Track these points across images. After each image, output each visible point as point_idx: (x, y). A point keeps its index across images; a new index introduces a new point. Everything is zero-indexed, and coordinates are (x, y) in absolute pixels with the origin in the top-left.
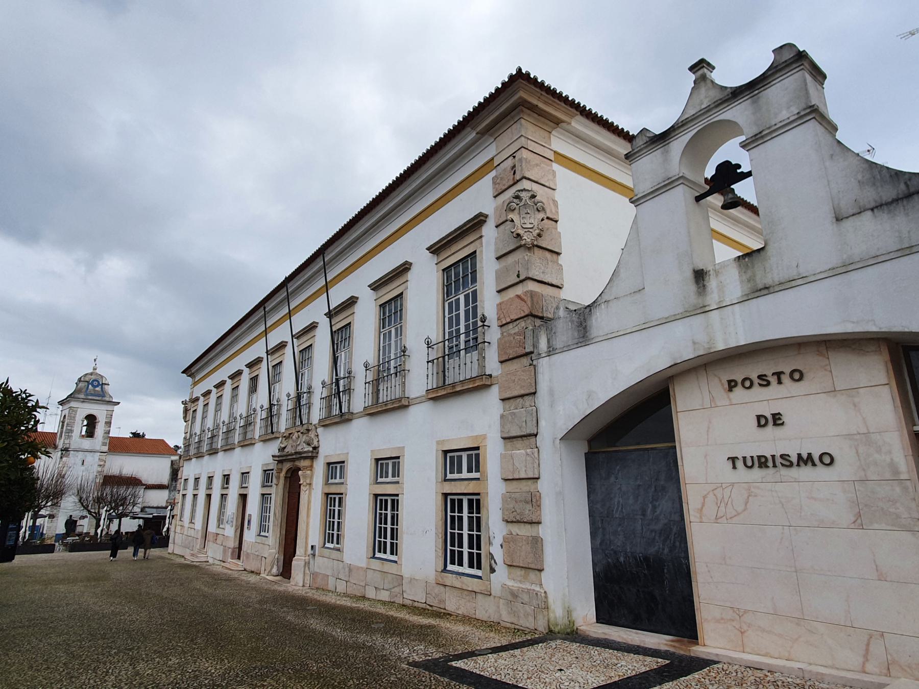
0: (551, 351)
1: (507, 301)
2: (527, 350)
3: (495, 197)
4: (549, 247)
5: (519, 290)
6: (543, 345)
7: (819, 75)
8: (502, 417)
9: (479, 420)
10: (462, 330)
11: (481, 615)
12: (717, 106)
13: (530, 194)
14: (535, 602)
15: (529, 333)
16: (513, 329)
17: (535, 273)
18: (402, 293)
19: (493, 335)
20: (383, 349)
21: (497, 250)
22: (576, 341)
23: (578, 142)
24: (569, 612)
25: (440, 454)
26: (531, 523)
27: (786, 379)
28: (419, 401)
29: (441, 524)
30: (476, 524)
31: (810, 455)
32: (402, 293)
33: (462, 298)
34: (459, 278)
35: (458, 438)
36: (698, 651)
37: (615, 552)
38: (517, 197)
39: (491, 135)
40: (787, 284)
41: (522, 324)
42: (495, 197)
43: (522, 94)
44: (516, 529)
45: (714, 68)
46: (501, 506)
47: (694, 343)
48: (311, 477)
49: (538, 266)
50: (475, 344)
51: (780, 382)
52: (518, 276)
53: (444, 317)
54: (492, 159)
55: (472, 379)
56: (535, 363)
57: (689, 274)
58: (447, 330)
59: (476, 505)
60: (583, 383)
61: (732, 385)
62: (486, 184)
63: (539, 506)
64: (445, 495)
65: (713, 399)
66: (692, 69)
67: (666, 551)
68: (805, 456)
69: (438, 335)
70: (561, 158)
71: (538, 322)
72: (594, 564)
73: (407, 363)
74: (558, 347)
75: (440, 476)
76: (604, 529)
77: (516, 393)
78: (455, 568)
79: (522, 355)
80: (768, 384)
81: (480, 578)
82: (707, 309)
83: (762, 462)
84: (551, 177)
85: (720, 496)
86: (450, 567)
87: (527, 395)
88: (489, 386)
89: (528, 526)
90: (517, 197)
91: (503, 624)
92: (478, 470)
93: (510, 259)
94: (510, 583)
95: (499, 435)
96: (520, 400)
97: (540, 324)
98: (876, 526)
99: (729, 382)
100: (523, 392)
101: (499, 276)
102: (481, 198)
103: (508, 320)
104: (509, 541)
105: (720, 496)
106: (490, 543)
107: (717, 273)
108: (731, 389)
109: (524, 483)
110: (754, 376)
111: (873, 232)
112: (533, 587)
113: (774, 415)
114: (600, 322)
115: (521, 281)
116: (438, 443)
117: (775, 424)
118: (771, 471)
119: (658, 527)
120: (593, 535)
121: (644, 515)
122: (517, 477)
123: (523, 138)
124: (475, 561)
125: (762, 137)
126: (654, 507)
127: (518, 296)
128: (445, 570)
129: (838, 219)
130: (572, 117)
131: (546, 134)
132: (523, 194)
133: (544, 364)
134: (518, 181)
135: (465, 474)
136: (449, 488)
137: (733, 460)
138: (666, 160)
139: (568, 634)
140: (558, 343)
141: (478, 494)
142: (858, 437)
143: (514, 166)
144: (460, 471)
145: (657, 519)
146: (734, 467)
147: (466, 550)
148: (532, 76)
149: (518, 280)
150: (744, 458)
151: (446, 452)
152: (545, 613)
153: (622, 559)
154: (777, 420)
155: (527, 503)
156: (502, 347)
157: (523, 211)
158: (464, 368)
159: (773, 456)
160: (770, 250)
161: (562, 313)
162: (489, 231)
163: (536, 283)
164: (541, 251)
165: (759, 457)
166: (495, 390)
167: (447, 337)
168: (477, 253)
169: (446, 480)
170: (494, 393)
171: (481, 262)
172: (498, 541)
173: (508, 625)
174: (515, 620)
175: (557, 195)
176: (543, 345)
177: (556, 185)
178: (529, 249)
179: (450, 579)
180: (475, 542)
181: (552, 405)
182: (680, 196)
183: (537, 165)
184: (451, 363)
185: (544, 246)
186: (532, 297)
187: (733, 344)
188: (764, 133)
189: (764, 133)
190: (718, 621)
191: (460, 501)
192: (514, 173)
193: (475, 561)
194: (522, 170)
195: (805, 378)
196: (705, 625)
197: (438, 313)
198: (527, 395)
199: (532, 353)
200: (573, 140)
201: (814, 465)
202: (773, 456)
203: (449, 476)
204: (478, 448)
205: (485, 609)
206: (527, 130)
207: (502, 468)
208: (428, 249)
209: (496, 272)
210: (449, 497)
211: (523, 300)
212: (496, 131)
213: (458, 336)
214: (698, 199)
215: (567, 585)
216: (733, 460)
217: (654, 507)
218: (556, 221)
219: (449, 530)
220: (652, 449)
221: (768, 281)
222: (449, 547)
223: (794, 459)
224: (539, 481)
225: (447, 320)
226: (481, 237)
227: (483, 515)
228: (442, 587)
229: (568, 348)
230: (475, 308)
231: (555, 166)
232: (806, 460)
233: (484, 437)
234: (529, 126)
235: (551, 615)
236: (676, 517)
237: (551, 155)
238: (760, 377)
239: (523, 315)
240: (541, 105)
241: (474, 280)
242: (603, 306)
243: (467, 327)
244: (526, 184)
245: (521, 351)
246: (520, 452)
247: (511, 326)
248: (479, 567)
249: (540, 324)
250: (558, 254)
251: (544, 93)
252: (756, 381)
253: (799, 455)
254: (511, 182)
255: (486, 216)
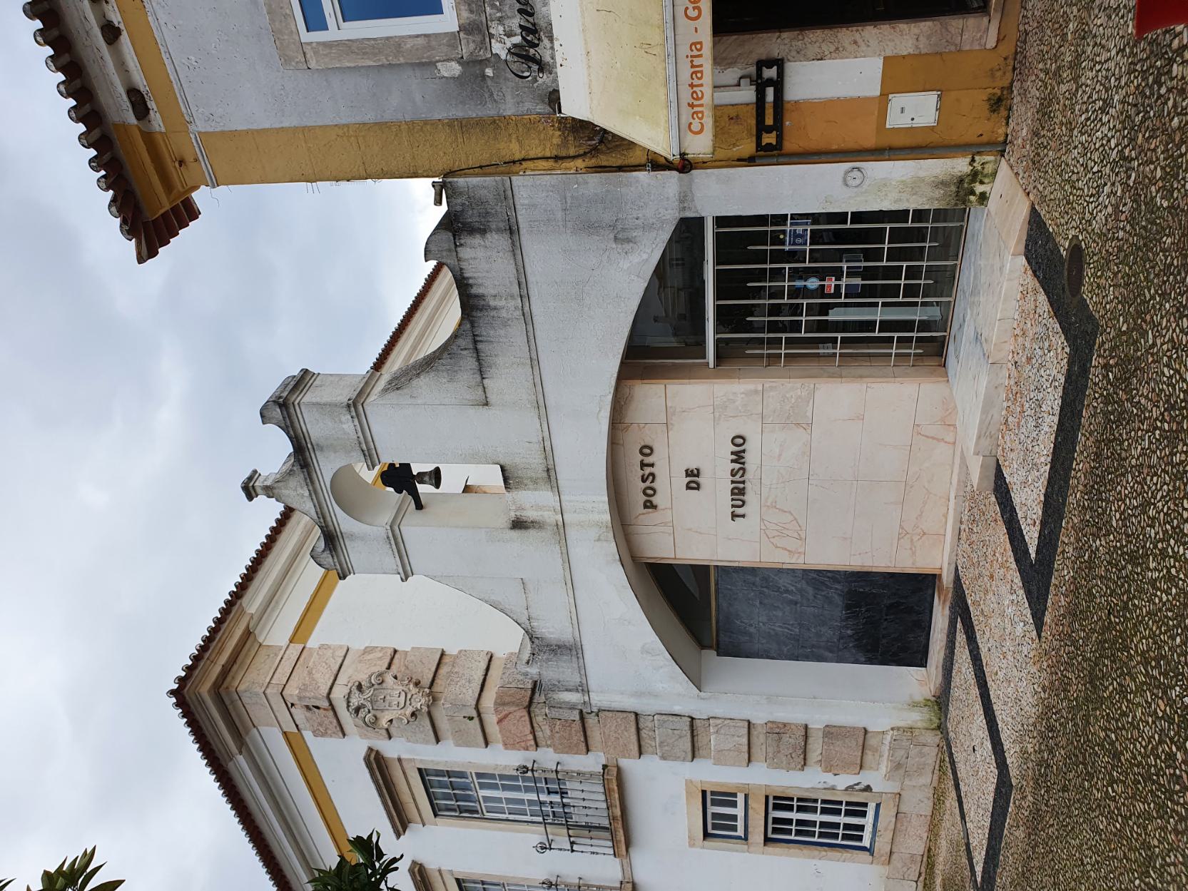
0: (583, 688)
1: (503, 736)
2: (577, 718)
3: (344, 735)
4: (433, 669)
5: (491, 719)
6: (574, 697)
7: (302, 380)
8: (663, 758)
9: (665, 791)
10: (533, 797)
11: (926, 808)
12: (312, 483)
13: (356, 692)
14: (906, 743)
15: (554, 713)
16: (544, 731)
17: (470, 695)
18: (458, 880)
19: (547, 758)
21: (427, 742)
22: (574, 659)
23: (277, 603)
24: (914, 705)
25: (709, 843)
26: (806, 737)
27: (648, 460)
28: (627, 867)
29: (807, 851)
30: (806, 805)
31: (732, 453)
32: (458, 880)
33: (483, 793)
34: (452, 796)
35: (688, 818)
36: (947, 579)
37: (841, 638)
38: (357, 710)
39: (247, 732)
40: (547, 452)
41: (539, 719)
42: (344, 735)
43: (205, 689)
44: (814, 755)
45: (255, 472)
46: (784, 771)
47: (599, 540)
49: (458, 690)
50: (556, 783)
51: (652, 465)
52: (471, 718)
53: (508, 820)
54: (285, 733)
55: (607, 792)
56: (595, 710)
57: (516, 534)
58: (528, 818)
59: (782, 802)
60: (627, 654)
61: (649, 505)
62: (322, 749)
63: (785, 725)
65: (665, 524)
66: (250, 498)
68: (734, 457)
69: (534, 832)
70: (301, 632)
71: (539, 698)
72: (856, 662)
73: (569, 881)
74: (578, 680)
75: (740, 846)
76: (813, 646)
77: (634, 738)
78: (867, 835)
79: (583, 726)
80: (653, 475)
81: (878, 806)
82: (560, 523)
83: (738, 492)
84: (329, 653)
85: (776, 533)
86: (866, 842)
87: (637, 724)
88: (619, 770)
89: (810, 740)
90: (357, 710)
91: (935, 784)
92: (735, 795)
93: (443, 724)
94: (883, 769)
95: (688, 764)
96: (644, 733)
97: (539, 695)
98: (809, 414)
99: (646, 507)
100: (633, 729)
101: (463, 741)
102: (341, 759)
103: (531, 737)
104: (829, 765)
105: (776, 533)
106: (833, 788)
107: (521, 508)
108: (654, 507)
109: (754, 739)
110: (643, 485)
111: (507, 379)
112: (887, 742)
113: (687, 475)
114: (554, 627)
115: (479, 715)
116: (692, 845)
117: (698, 476)
118: (748, 485)
119: (810, 590)
120: (820, 659)
121: (796, 603)
122: (746, 748)
123: (268, 691)
124: (857, 810)
125: (369, 450)
126: (787, 591)
127: (500, 721)
128: (869, 850)
129: (487, 404)
130: (243, 611)
131: (263, 652)
132: (355, 702)
133: (598, 700)
134: (331, 704)
135: (739, 811)
136: (757, 835)
137: (734, 516)
138: (362, 538)
139: (940, 709)
140: (573, 678)
141: (767, 797)
142: (717, 414)
143: (307, 707)
144: (734, 818)
145: (801, 591)
146: (743, 516)
147: (842, 819)
148: (183, 674)
149: (476, 720)
150: (733, 506)
151: (706, 835)
152: (916, 733)
153: (849, 632)
154: (693, 474)
155: (780, 739)
156: (569, 749)
157: (380, 705)
158: (589, 801)
159: (733, 482)
160: (506, 461)
162: (391, 749)
163: (485, 694)
164: (437, 681)
165: (733, 494)
166: (625, 763)
167: (540, 819)
169: (746, 839)
170: (631, 766)
171: (438, 763)
172: (830, 779)
173: (936, 777)
174: (929, 769)
175: (357, 645)
176: (574, 697)
177: (341, 647)
178: (434, 699)
179: (882, 845)
180: (831, 807)
181: (656, 696)
182: (415, 530)
183: (310, 673)
184: (578, 817)
185: (431, 676)
186: (504, 704)
187: (607, 507)
188: (364, 448)
189: (364, 448)
190: (914, 553)
191: (776, 820)
192: (317, 708)
193: (857, 810)
194: (316, 698)
195: (650, 444)
196: (919, 565)
197: (500, 829)
198: (637, 724)
199: (581, 712)
200: (273, 610)
201: (744, 451)
202: (733, 482)
203: (740, 832)
204: (704, 792)
205: (918, 803)
206: (253, 683)
207: (733, 765)
208: (398, 836)
209: (458, 745)
210: (770, 835)
211: (506, 716)
212: (242, 721)
213: (542, 803)
214: (419, 506)
215: (881, 698)
216: (734, 516)
217: (787, 591)
218: (395, 651)
219: (816, 839)
220: (717, 584)
221: (542, 468)
222: (839, 841)
223: (737, 466)
224: (753, 721)
225: (511, 817)
226: (399, 760)
227: (796, 794)
228: (894, 857)
229: (582, 670)
230: (502, 777)
231: (313, 643)
232: (739, 457)
233: (689, 783)
234: (252, 676)
235: (920, 725)
237: (295, 649)
238: (644, 480)
239: (527, 718)
240: (223, 659)
241: (462, 775)
242: (535, 624)
243: (527, 790)
244: (339, 694)
245: (578, 725)
246: (713, 740)
247: (539, 734)
248: (866, 805)
249: (539, 695)
250: (443, 654)
251: (207, 655)
252: (648, 484)
253: (733, 461)
254: (331, 713)
255: (370, 749)
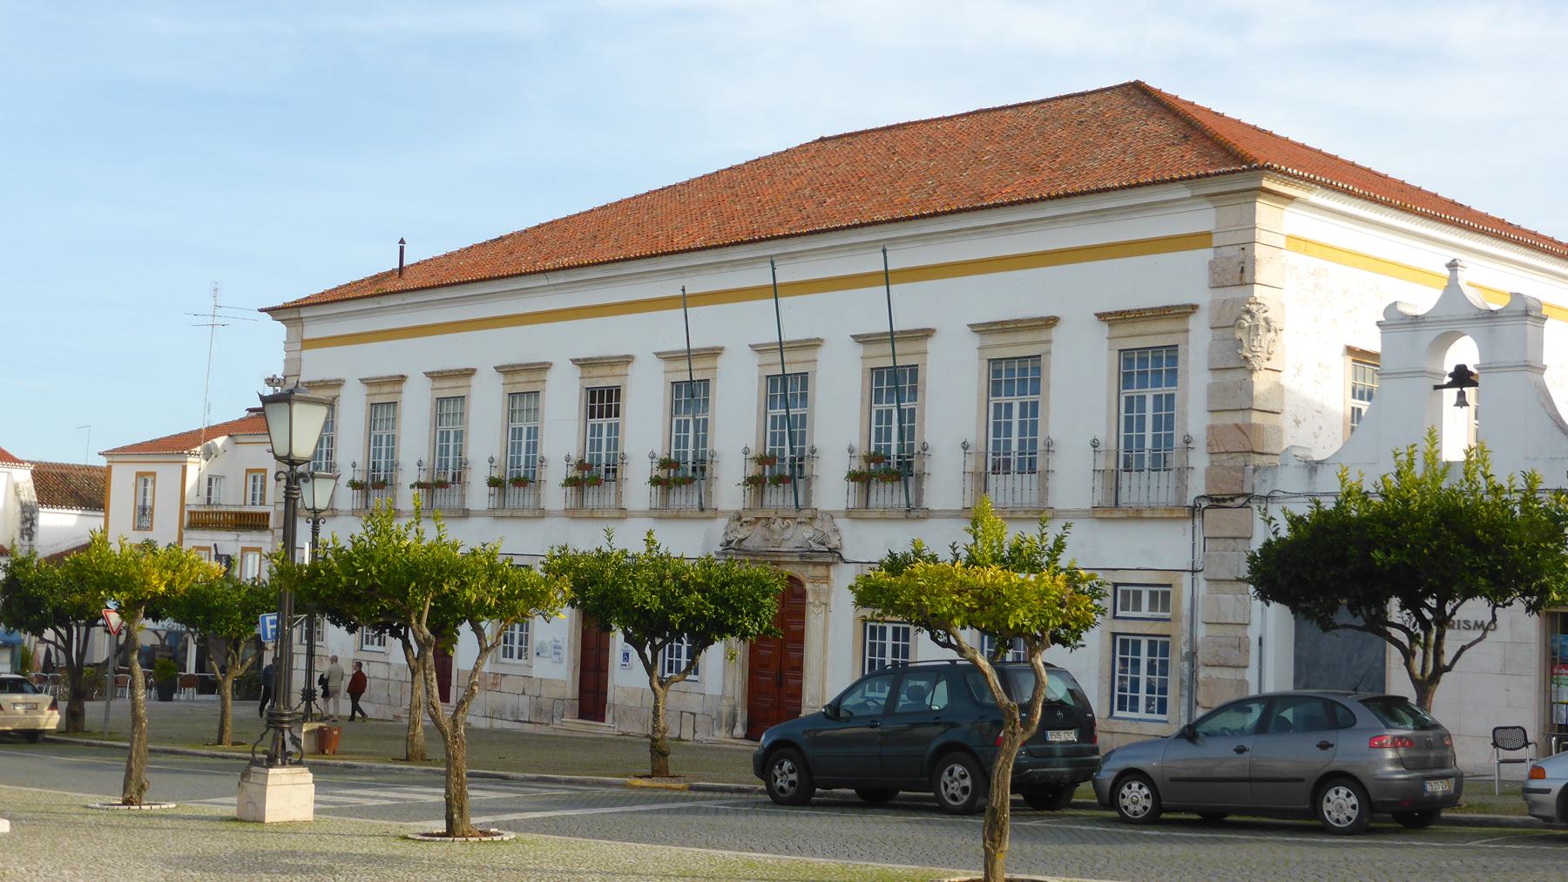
20: (373, 441)
21: (1211, 359)
48: (828, 593)
64: (1114, 635)
67: (163, 588)
161: (1293, 462)
168: (1180, 349)
236: (1378, 665)
247: (1224, 457)
